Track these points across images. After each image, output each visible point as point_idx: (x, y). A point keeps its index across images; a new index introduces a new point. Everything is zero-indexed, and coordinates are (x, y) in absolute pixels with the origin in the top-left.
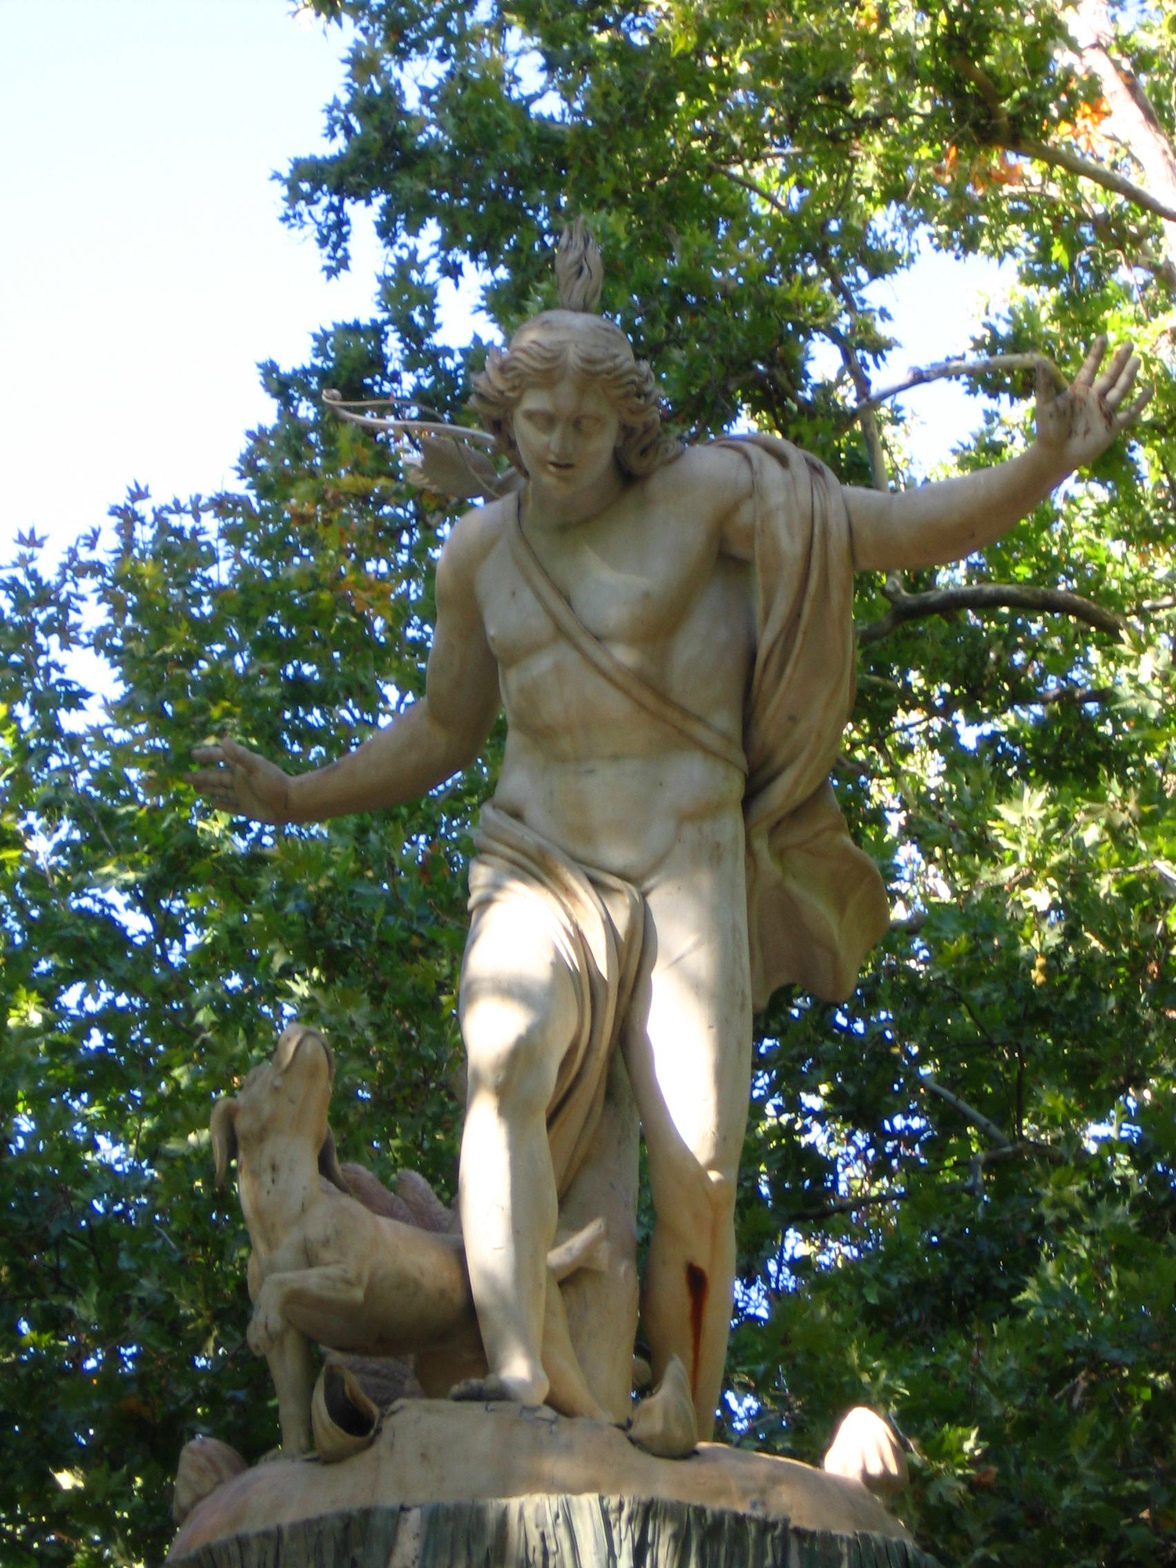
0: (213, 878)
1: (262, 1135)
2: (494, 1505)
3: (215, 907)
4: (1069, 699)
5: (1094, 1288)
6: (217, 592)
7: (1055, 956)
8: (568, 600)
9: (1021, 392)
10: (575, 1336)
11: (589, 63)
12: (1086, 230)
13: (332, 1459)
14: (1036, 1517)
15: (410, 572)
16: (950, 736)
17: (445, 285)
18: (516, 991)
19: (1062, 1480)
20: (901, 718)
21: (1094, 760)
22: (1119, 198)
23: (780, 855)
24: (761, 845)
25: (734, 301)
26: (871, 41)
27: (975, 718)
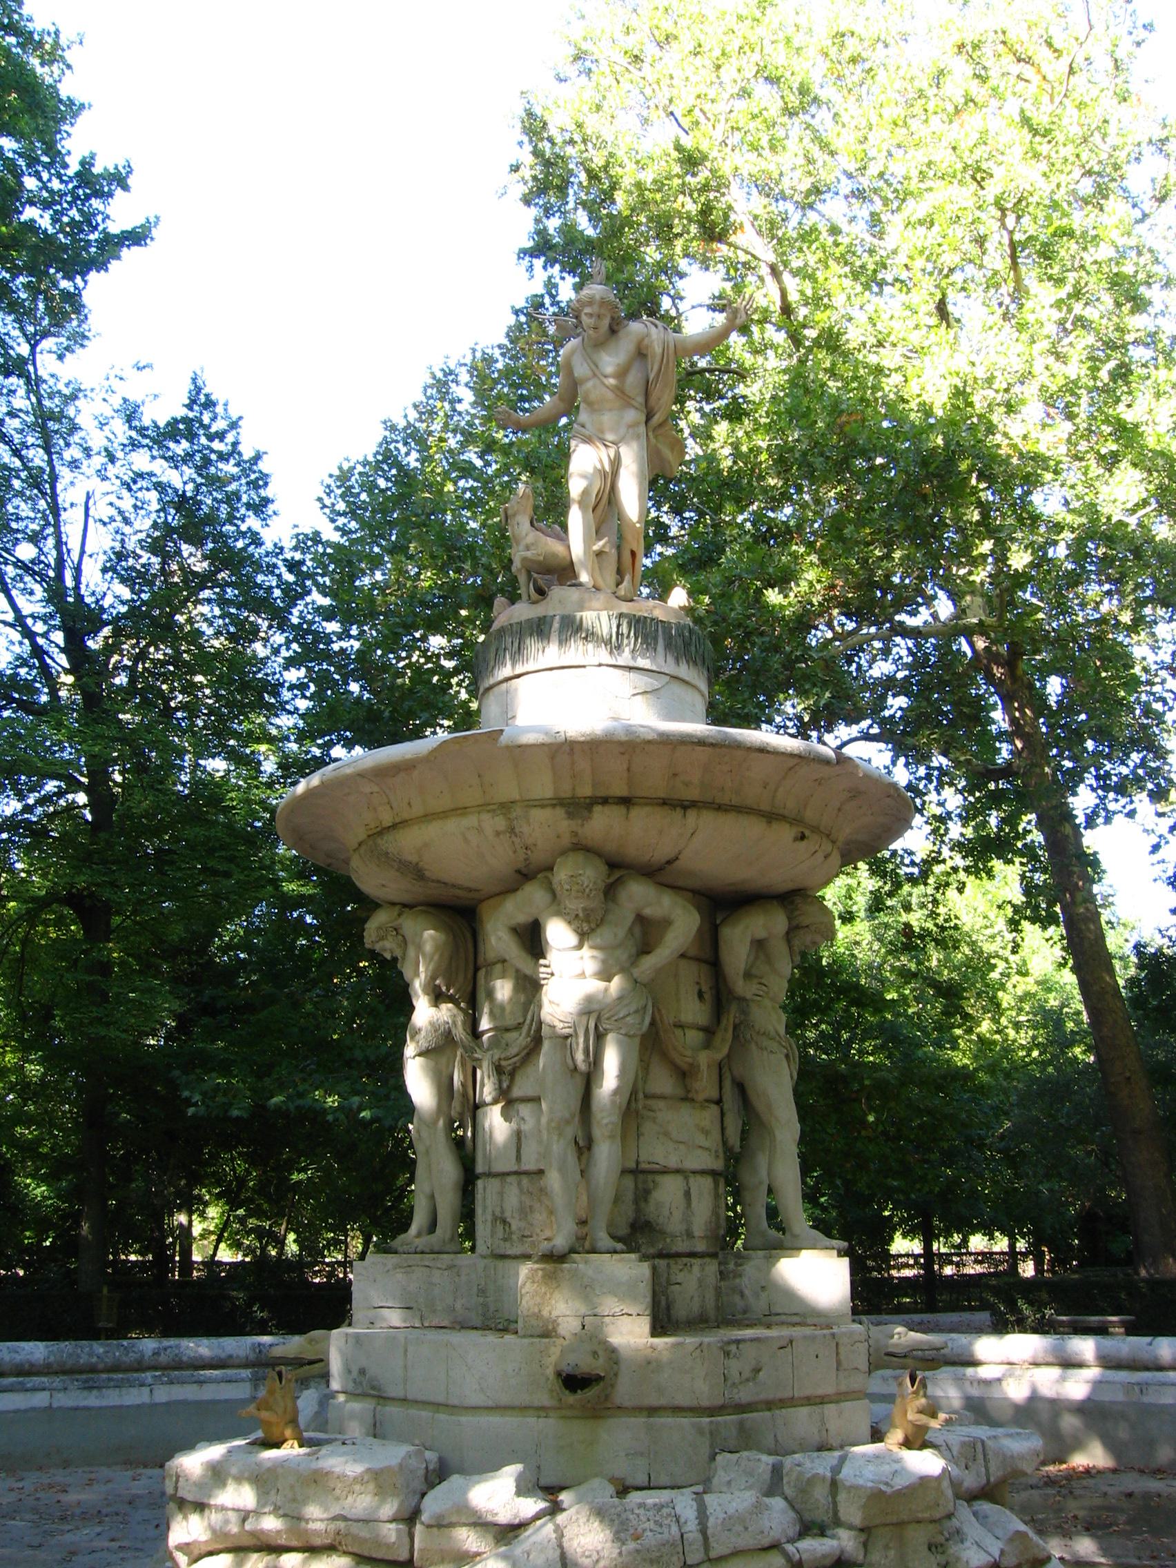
0: (500, 450)
1: (514, 515)
2: (578, 615)
3: (500, 459)
4: (734, 398)
5: (740, 559)
6: (499, 371)
7: (731, 468)
8: (597, 366)
9: (722, 311)
10: (600, 569)
11: (601, 219)
12: (739, 266)
13: (534, 603)
14: (724, 620)
15: (552, 364)
16: (701, 408)
17: (561, 283)
18: (584, 476)
19: (732, 610)
20: (688, 403)
21: (741, 415)
22: (749, 257)
23: (656, 437)
24: (650, 434)
25: (641, 286)
26: (679, 212)
27: (708, 403)
